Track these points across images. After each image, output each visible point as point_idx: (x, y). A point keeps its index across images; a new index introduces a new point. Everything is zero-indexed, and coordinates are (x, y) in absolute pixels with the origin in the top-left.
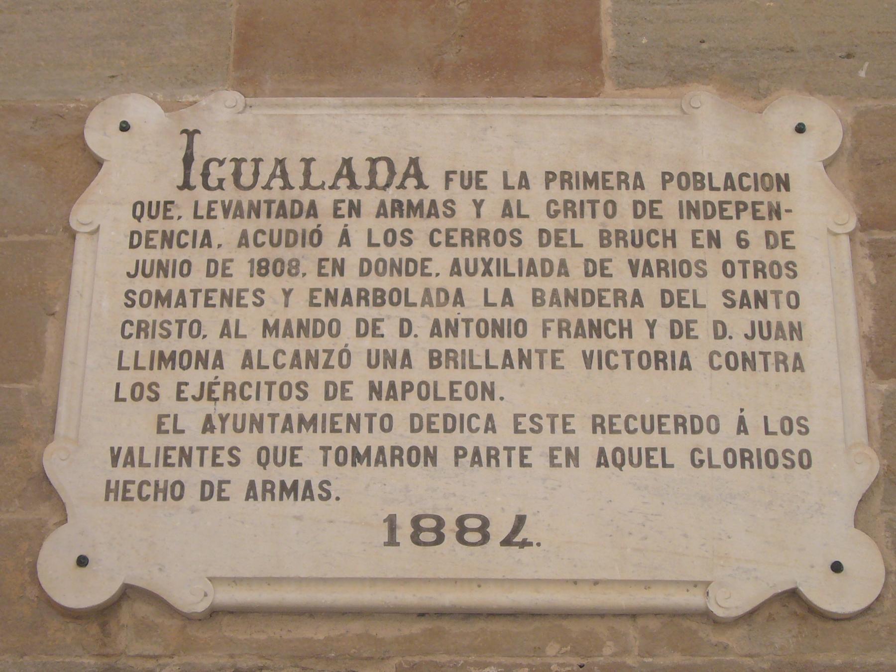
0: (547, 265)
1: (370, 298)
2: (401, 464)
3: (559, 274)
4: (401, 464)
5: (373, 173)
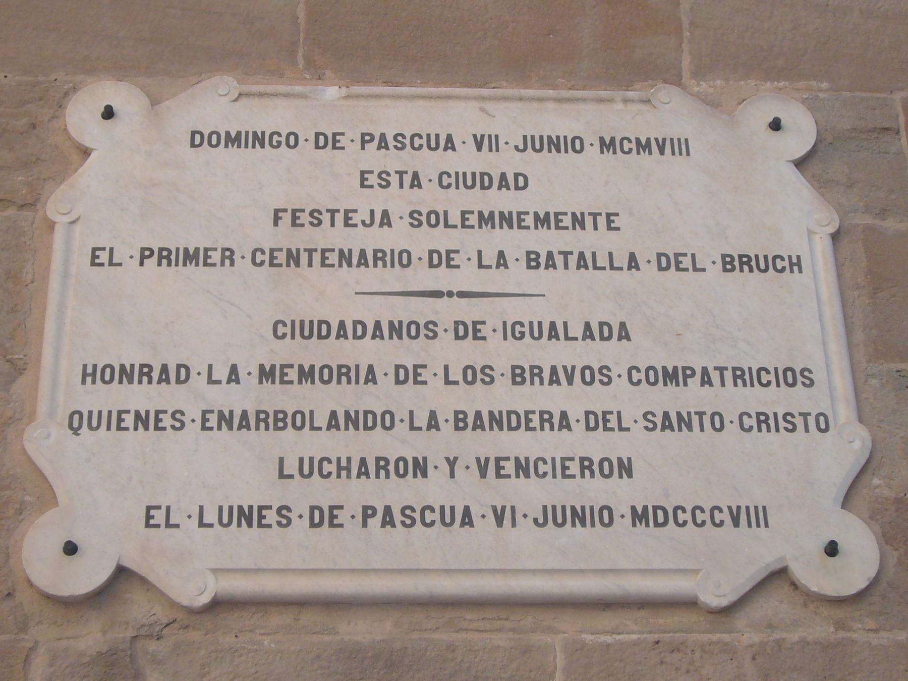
0: (606, 329)
1: (271, 420)
2: (387, 476)
3: (620, 339)
4: (387, 476)
5: (516, 180)
